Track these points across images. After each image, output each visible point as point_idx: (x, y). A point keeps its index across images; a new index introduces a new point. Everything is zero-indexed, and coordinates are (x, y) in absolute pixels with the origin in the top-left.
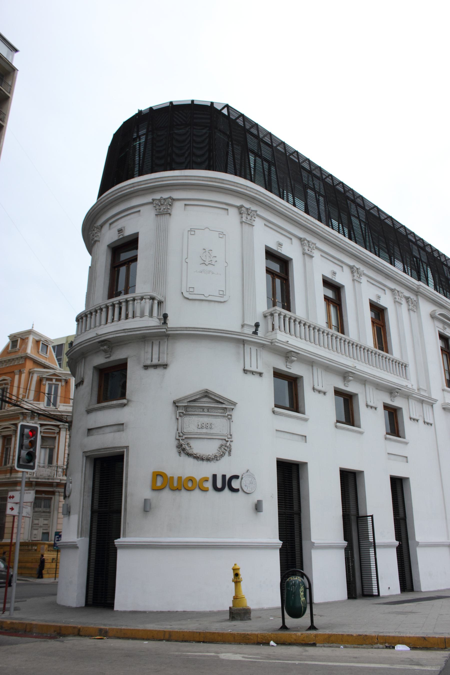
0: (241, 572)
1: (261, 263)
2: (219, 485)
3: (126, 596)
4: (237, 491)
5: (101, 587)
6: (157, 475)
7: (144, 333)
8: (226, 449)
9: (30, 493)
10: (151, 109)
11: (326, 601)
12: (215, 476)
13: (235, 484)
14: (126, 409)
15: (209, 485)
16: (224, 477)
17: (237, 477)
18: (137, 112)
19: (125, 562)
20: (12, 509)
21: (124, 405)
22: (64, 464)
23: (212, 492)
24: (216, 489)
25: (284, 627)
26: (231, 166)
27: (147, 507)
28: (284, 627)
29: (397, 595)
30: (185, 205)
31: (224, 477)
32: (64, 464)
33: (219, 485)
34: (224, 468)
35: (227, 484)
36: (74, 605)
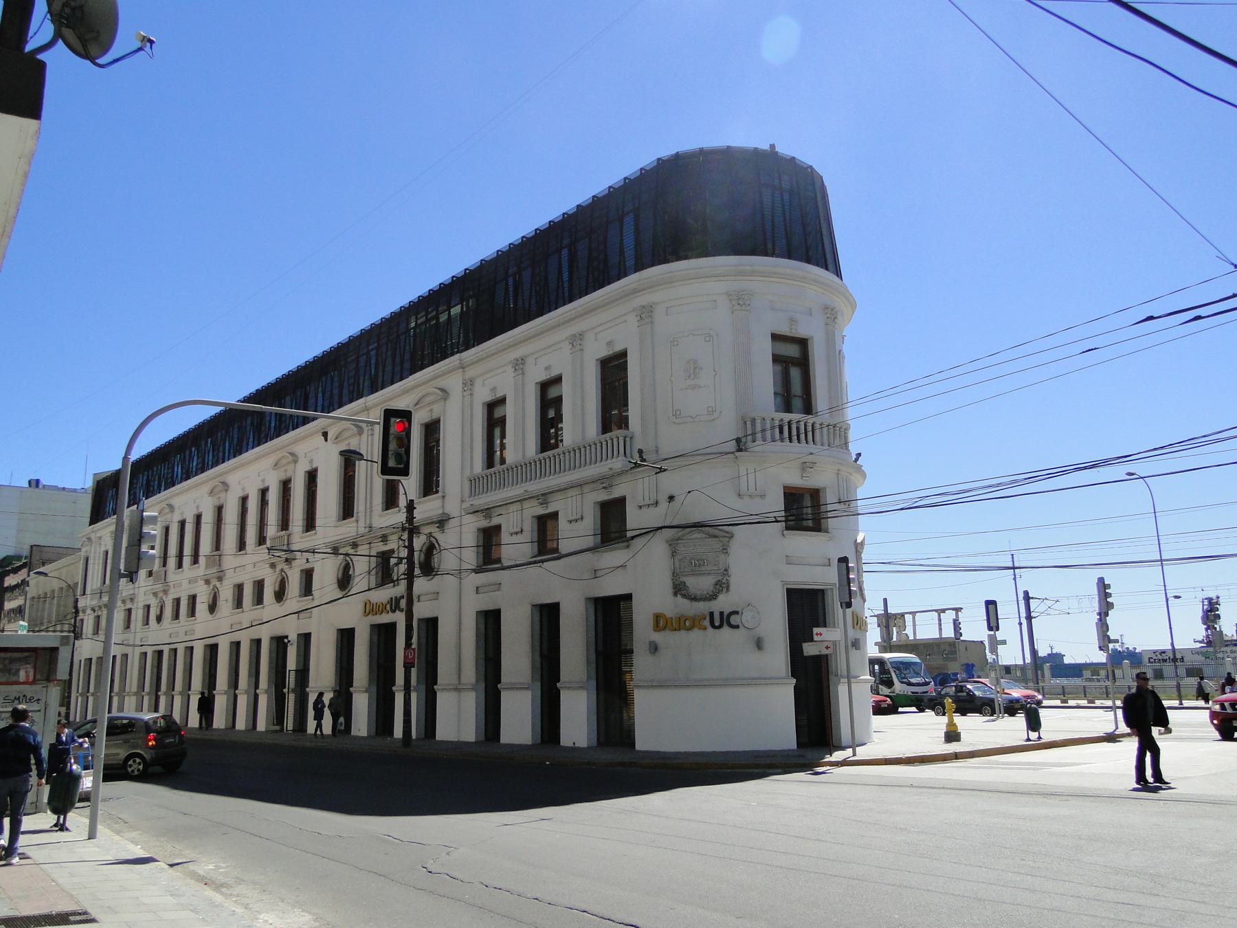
0: (1222, 610)
1: (764, 350)
2: (717, 624)
4: (737, 627)
6: (657, 617)
7: (270, 668)
8: (722, 586)
10: (756, 149)
12: (712, 614)
13: (734, 619)
15: (707, 623)
16: (722, 613)
17: (736, 613)
18: (766, 147)
23: (710, 630)
25: (1029, 740)
28: (1029, 740)
31: (722, 613)
33: (717, 624)
34: (723, 603)
35: (725, 620)
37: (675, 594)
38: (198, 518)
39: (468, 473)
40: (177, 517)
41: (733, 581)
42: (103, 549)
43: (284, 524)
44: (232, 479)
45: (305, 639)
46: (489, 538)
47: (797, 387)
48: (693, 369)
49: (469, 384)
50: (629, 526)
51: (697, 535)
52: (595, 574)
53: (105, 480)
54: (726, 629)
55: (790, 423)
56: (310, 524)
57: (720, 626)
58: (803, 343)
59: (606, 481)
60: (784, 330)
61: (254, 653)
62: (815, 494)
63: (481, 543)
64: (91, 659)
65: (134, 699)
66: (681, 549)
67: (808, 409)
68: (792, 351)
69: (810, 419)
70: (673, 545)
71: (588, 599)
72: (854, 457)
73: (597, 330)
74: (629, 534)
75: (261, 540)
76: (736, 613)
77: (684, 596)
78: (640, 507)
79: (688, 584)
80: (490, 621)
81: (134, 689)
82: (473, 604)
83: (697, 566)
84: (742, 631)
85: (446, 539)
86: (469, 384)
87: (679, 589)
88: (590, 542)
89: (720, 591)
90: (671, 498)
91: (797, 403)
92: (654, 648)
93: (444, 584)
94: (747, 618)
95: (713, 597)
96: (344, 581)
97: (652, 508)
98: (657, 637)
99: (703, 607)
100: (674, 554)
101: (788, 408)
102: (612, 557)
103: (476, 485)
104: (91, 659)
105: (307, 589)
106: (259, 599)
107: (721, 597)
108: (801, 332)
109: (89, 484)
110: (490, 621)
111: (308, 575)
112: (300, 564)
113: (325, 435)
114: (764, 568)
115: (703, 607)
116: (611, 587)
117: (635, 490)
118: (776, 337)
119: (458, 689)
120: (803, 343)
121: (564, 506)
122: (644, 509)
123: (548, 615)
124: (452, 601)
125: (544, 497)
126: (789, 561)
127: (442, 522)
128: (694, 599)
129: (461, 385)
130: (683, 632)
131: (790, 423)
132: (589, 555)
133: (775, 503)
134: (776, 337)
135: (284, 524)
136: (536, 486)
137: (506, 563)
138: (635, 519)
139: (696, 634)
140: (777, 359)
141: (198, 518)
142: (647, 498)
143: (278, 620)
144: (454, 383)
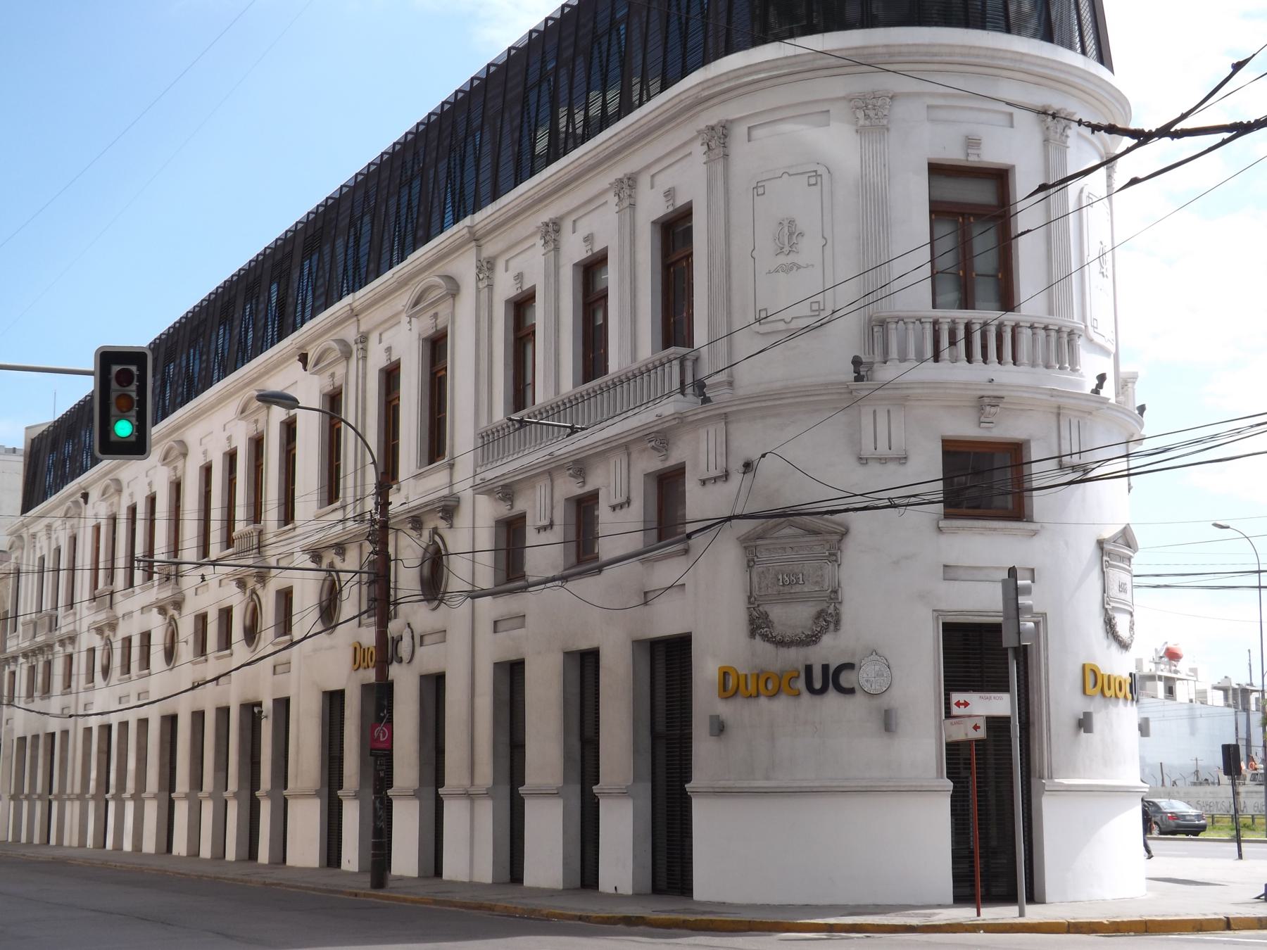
3: (712, 878)
4: (851, 691)
5: (670, 864)
8: (828, 620)
9: (1001, 698)
11: (753, 902)
12: (809, 669)
14: (1036, 542)
15: (801, 684)
16: (825, 668)
17: (850, 666)
19: (706, 820)
20: (976, 728)
21: (1035, 533)
22: (332, 647)
23: (806, 696)
24: (811, 689)
26: (852, 11)
27: (1084, 723)
29: (551, 893)
30: (928, 107)
31: (825, 668)
32: (332, 647)
33: (818, 685)
34: (829, 650)
35: (832, 680)
36: (630, 892)
37: (752, 634)
38: (152, 500)
39: (484, 423)
40: (125, 502)
41: (848, 613)
42: (38, 555)
43: (256, 514)
44: (192, 436)
45: (283, 705)
46: (511, 532)
47: (984, 262)
48: (789, 235)
49: (486, 267)
50: (689, 517)
51: (788, 531)
52: (646, 598)
53: (41, 437)
54: (832, 697)
55: (968, 327)
56: (288, 515)
57: (823, 690)
58: (1000, 177)
59: (660, 438)
60: (953, 154)
61: (168, 738)
62: (1015, 452)
63: (572, 536)
64: (24, 739)
65: (77, 804)
66: (764, 556)
67: (1007, 300)
68: (980, 194)
69: (1009, 318)
70: (749, 545)
71: (637, 644)
72: (1093, 383)
73: (653, 171)
74: (690, 528)
75: (229, 542)
76: (850, 666)
77: (765, 638)
78: (704, 482)
79: (772, 616)
80: (512, 674)
81: (77, 790)
82: (491, 650)
83: (788, 588)
84: (859, 698)
85: (457, 539)
86: (486, 267)
87: (758, 625)
88: (635, 542)
89: (824, 630)
90: (748, 466)
91: (985, 289)
92: (719, 728)
93: (456, 614)
94: (867, 676)
95: (812, 639)
96: (328, 612)
97: (720, 484)
98: (724, 709)
99: (794, 657)
100: (750, 564)
101: (966, 302)
102: (667, 571)
103: (489, 441)
104: (53, 734)
105: (285, 623)
106: (226, 642)
107: (827, 640)
108: (992, 155)
109: (20, 443)
110: (512, 674)
111: (285, 597)
112: (277, 581)
113: (304, 358)
114: (905, 583)
115: (794, 657)
116: (666, 623)
117: (697, 452)
118: (936, 170)
119: (469, 796)
120: (1000, 177)
121: (608, 481)
122: (710, 487)
123: (585, 665)
124: (458, 642)
125: (579, 468)
126: (950, 572)
127: (448, 509)
128: (781, 643)
129: (474, 271)
130: (763, 701)
131: (968, 327)
132: (633, 566)
133: (927, 466)
134: (936, 170)
135: (256, 514)
136: (565, 447)
137: (531, 580)
138: (700, 502)
139: (780, 706)
140: (938, 211)
141: (152, 500)
142: (712, 466)
143: (248, 678)
144: (465, 267)
